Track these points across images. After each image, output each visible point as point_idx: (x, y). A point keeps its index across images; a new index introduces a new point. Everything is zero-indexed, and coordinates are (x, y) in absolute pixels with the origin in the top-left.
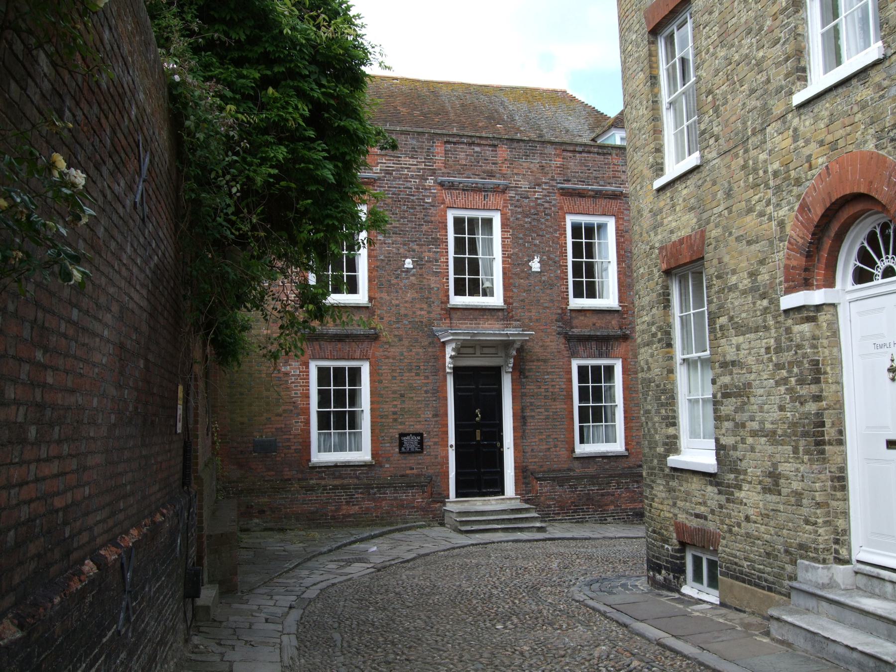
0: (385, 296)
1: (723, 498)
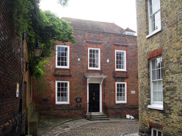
0: (73, 67)
1: (165, 117)
